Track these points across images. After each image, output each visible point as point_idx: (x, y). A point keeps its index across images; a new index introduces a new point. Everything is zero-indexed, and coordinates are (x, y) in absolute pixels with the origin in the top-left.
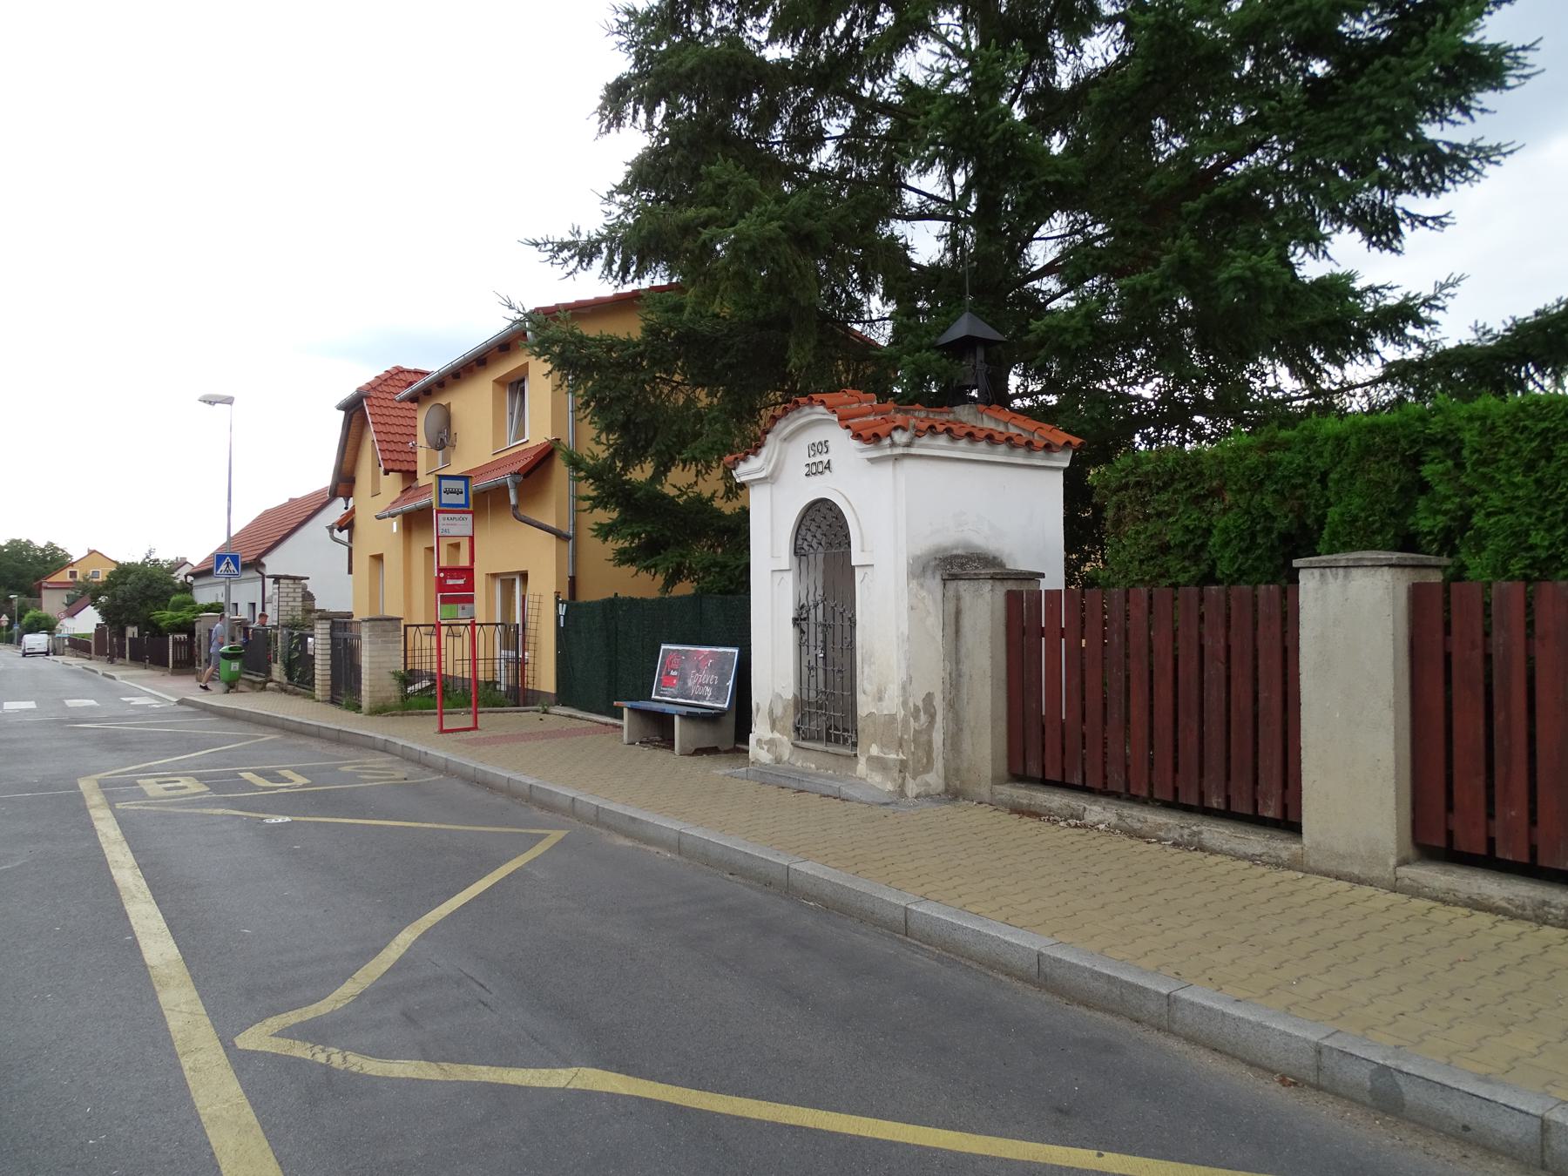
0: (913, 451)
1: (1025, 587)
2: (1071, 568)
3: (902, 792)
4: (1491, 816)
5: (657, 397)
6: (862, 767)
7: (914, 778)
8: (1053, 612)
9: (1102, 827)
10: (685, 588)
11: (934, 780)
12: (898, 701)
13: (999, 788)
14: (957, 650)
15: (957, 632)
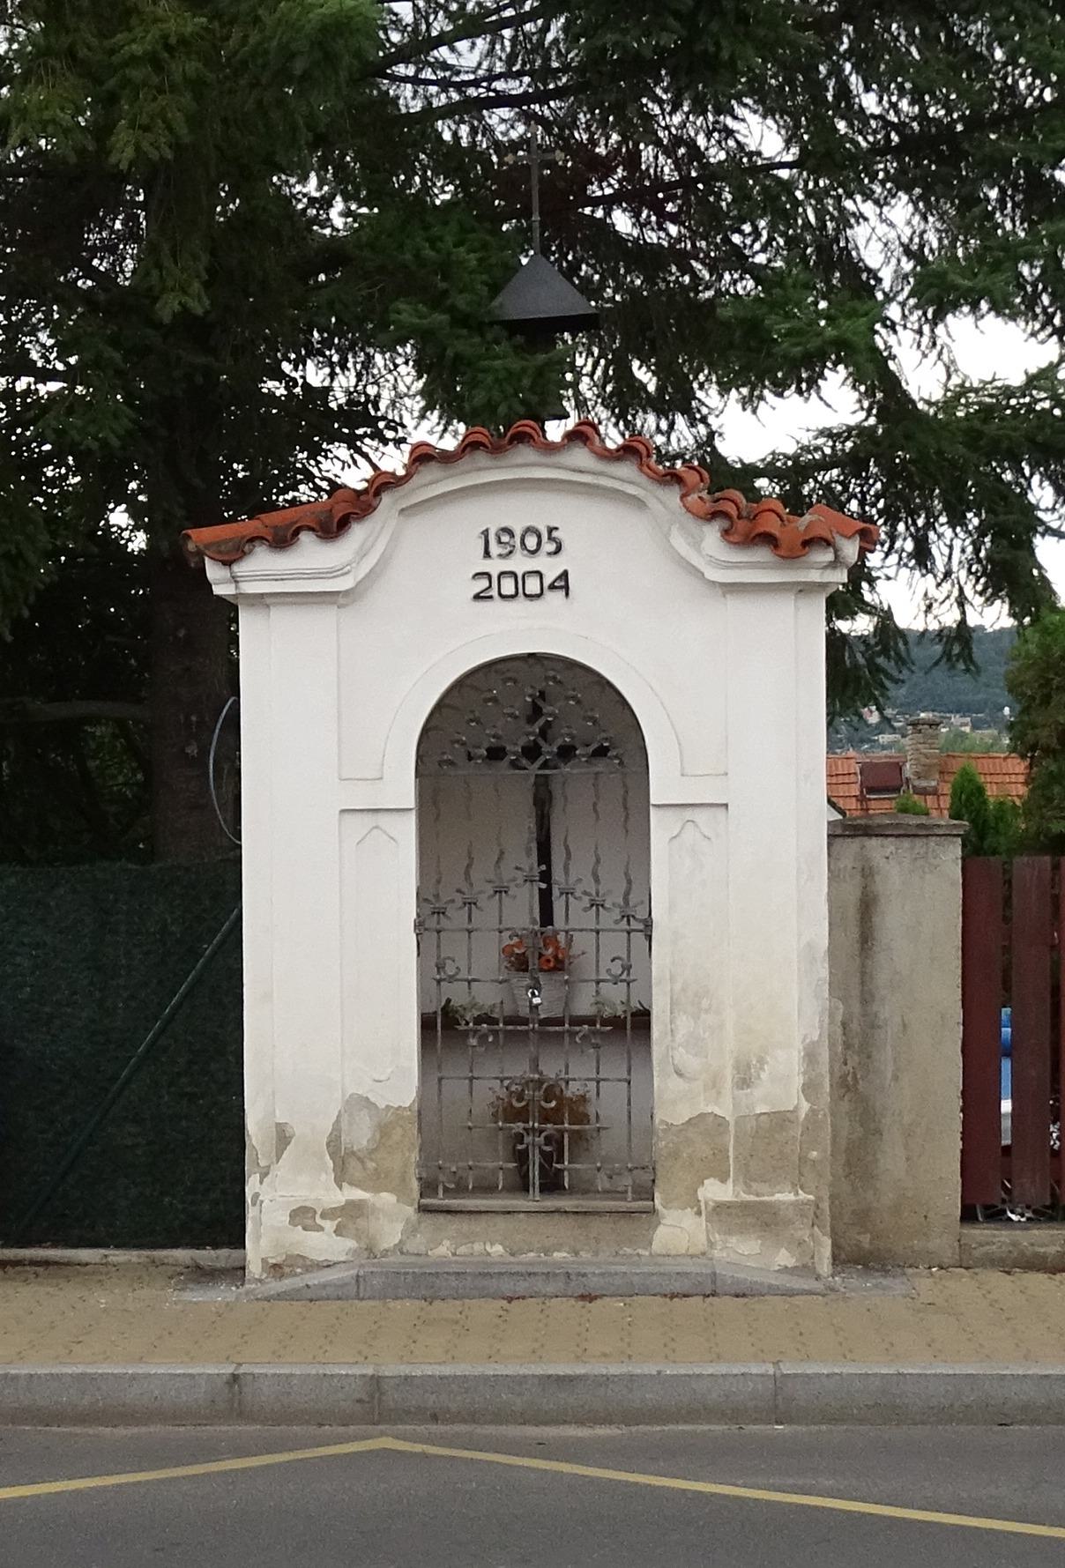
14: (865, 976)
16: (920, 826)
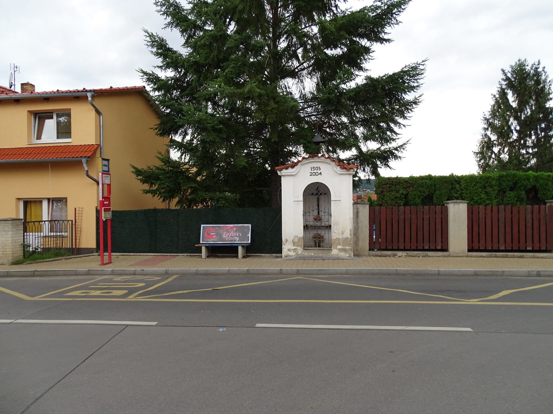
4: (479, 243)
14: (357, 221)
15: (357, 217)
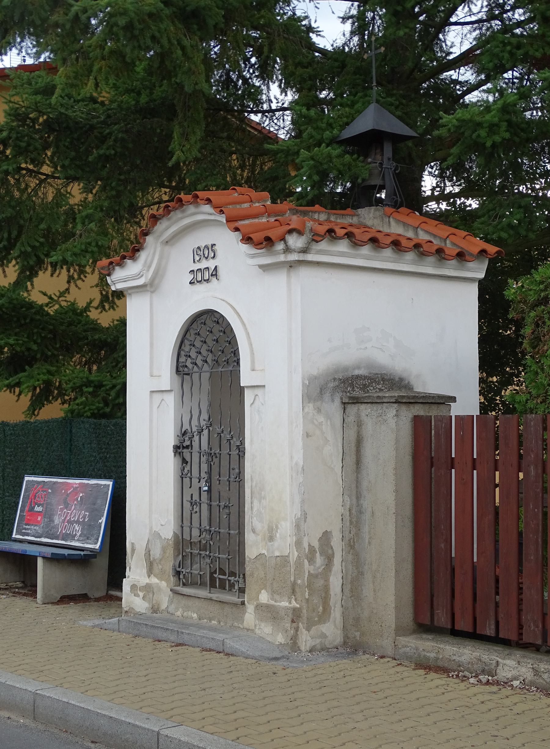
0: (310, 257)
1: (434, 412)
2: (487, 390)
3: (294, 645)
5: (22, 191)
6: (250, 616)
7: (308, 629)
8: (464, 440)
9: (516, 683)
10: (53, 411)
11: (332, 630)
12: (291, 540)
13: (403, 640)
14: (358, 482)
15: (358, 462)
16: (378, 397)
